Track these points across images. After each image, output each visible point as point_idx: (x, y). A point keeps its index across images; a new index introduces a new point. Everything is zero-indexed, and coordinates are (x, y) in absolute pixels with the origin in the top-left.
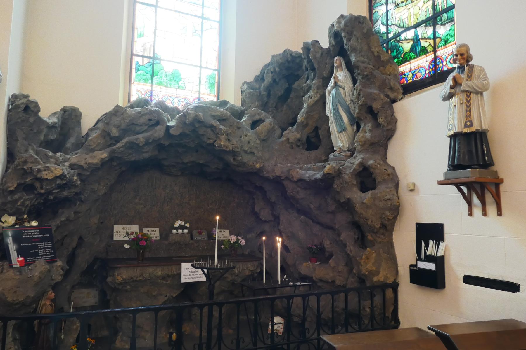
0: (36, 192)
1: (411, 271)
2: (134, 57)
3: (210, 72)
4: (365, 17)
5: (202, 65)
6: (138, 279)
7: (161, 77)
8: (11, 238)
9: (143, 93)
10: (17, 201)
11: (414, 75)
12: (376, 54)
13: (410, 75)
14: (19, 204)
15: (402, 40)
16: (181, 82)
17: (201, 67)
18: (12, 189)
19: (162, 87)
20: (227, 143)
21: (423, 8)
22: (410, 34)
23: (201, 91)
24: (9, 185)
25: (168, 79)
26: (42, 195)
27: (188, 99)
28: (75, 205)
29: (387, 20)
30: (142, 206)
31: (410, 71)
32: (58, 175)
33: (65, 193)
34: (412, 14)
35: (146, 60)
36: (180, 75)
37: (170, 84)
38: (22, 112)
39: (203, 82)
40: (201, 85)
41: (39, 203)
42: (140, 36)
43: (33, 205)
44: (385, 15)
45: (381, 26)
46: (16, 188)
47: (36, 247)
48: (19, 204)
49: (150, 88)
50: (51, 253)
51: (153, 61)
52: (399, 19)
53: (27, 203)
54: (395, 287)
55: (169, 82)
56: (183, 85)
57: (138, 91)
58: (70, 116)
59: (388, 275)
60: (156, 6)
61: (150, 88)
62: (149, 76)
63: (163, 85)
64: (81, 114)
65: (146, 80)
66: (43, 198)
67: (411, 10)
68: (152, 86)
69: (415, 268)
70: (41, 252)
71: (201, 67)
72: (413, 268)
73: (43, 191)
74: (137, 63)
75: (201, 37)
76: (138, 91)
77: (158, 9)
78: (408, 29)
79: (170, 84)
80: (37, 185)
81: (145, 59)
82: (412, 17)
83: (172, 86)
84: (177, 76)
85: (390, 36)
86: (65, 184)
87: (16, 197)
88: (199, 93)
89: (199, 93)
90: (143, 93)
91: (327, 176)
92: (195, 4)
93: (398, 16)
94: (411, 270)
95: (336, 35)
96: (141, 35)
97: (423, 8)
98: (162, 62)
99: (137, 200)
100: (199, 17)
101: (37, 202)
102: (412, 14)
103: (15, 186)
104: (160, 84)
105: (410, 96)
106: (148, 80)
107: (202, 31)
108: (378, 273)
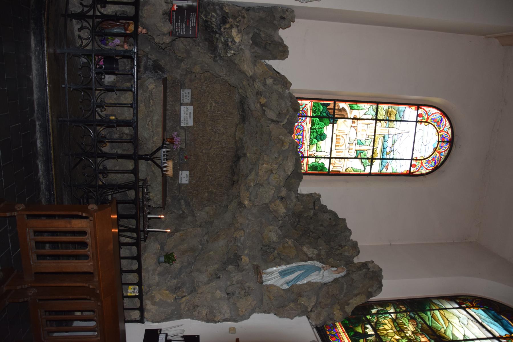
0: (221, 25)
1: (157, 330)
2: (333, 103)
3: (327, 166)
4: (380, 287)
5: (332, 159)
6: (151, 101)
7: (318, 124)
8: (191, 4)
9: (304, 109)
10: (215, 11)
11: (333, 335)
12: (351, 301)
13: (333, 332)
14: (213, 14)
15: (364, 326)
16: (316, 141)
17: (330, 158)
18: (224, 9)
19: (310, 125)
20: (264, 170)
21: (392, 339)
22: (370, 331)
23: (310, 159)
24: (227, 8)
25: (317, 130)
26: (220, 29)
27: (302, 147)
28: (211, 54)
29: (382, 314)
30: (209, 108)
31: (336, 333)
32: (235, 39)
33: (220, 46)
34: (388, 331)
35: (331, 112)
36: (322, 140)
37: (313, 132)
38: (283, 16)
39: (317, 160)
40: (314, 159)
41: (213, 28)
42: (350, 107)
43: (212, 24)
44: (386, 311)
45: (377, 310)
46: (225, 11)
47: (182, 21)
48: (213, 14)
49: (309, 115)
50: (176, 32)
51: (331, 118)
52: (383, 322)
53: (214, 19)
54: (141, 321)
55: (315, 131)
56: (314, 142)
57: (306, 105)
58: (282, 52)
59: (151, 314)
60: (376, 120)
61: (309, 115)
62: (319, 114)
63: (312, 126)
64: (283, 59)
65: (314, 112)
66: (217, 30)
67: (391, 331)
68: (310, 117)
69: (159, 333)
70: (178, 24)
71: (330, 158)
72: (159, 331)
73: (222, 30)
74: (329, 104)
75: (355, 158)
76: (306, 105)
77: (374, 121)
78: (374, 329)
79: (313, 132)
80: (227, 26)
81: (333, 111)
82: (385, 332)
83: (312, 134)
84: (320, 138)
85: (368, 317)
86: (228, 45)
87: (218, 12)
88: (308, 157)
89: (308, 157)
90: (304, 109)
91: (240, 259)
92: (383, 152)
93: (386, 321)
94: (158, 329)
95: (365, 265)
96: (352, 108)
97: (392, 339)
98: (332, 125)
99: (214, 104)
100: (372, 155)
101: (214, 26)
102: (388, 331)
103: (227, 11)
104: (313, 123)
105: (269, 4)
106: (315, 113)
107: (361, 159)
108: (154, 304)
